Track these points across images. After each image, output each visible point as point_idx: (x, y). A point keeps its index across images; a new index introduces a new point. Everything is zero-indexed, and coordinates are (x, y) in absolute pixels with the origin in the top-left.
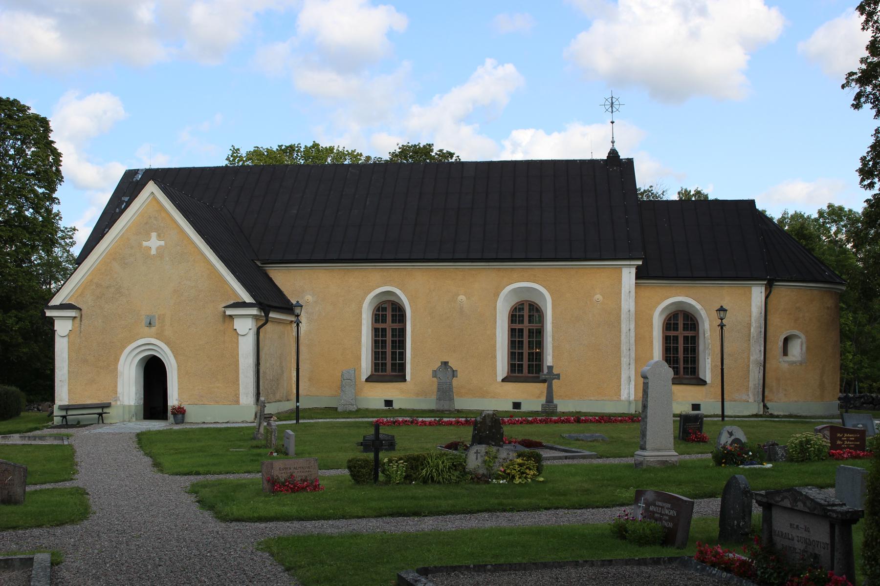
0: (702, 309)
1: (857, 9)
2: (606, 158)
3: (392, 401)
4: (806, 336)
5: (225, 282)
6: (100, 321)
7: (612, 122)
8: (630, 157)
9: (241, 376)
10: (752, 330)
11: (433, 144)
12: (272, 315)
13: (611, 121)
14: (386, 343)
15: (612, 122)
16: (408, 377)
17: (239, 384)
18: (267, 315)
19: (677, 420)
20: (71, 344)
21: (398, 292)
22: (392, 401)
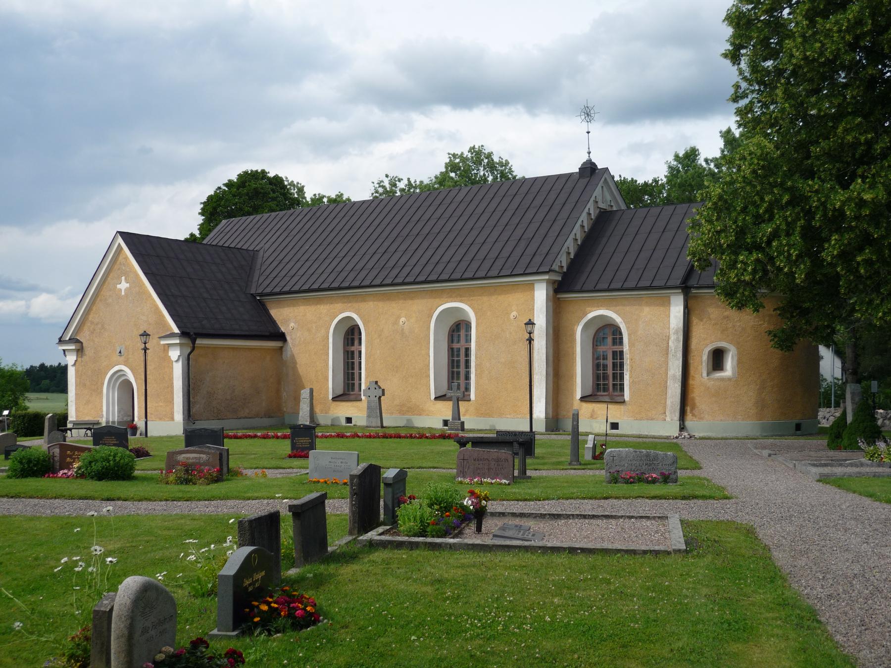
0: (621, 322)
1: (724, 21)
2: (577, 170)
3: (618, 423)
4: (738, 348)
5: (163, 316)
6: (93, 352)
7: (588, 132)
8: (190, 233)
9: (175, 396)
10: (671, 343)
11: (492, 153)
12: (199, 342)
13: (587, 131)
14: (622, 357)
15: (588, 132)
16: (473, 397)
17: (173, 403)
18: (194, 342)
19: (115, 418)
20: (77, 371)
21: (355, 316)
22: (618, 423)
